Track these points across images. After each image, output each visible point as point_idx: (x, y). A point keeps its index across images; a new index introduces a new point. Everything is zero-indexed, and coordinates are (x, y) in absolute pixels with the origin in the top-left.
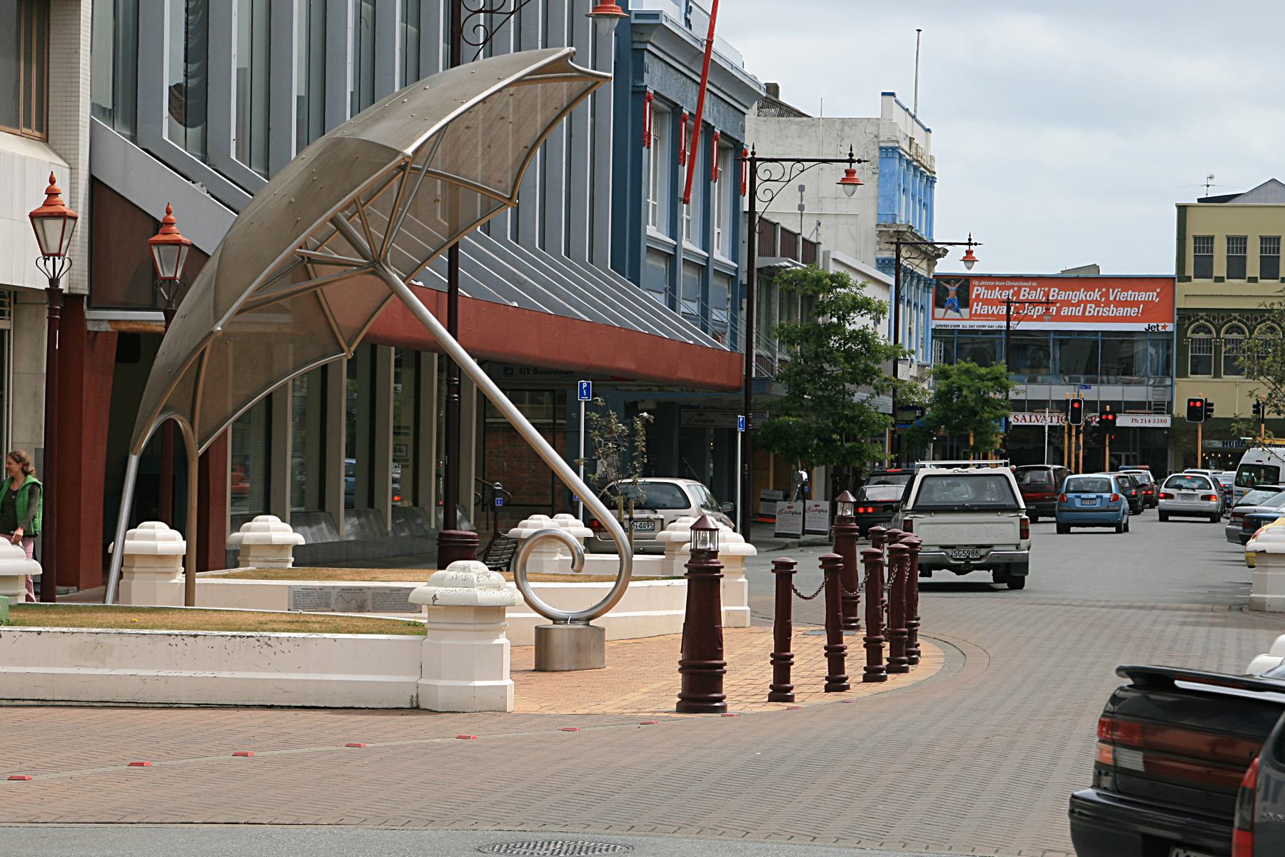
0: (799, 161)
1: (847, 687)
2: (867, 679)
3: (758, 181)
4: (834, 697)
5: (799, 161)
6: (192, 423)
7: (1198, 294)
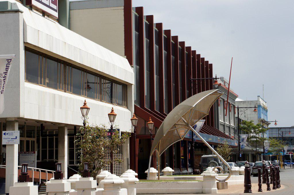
0: (246, 108)
1: (270, 190)
2: (273, 189)
3: (239, 111)
4: (268, 191)
5: (246, 108)
6: (158, 151)
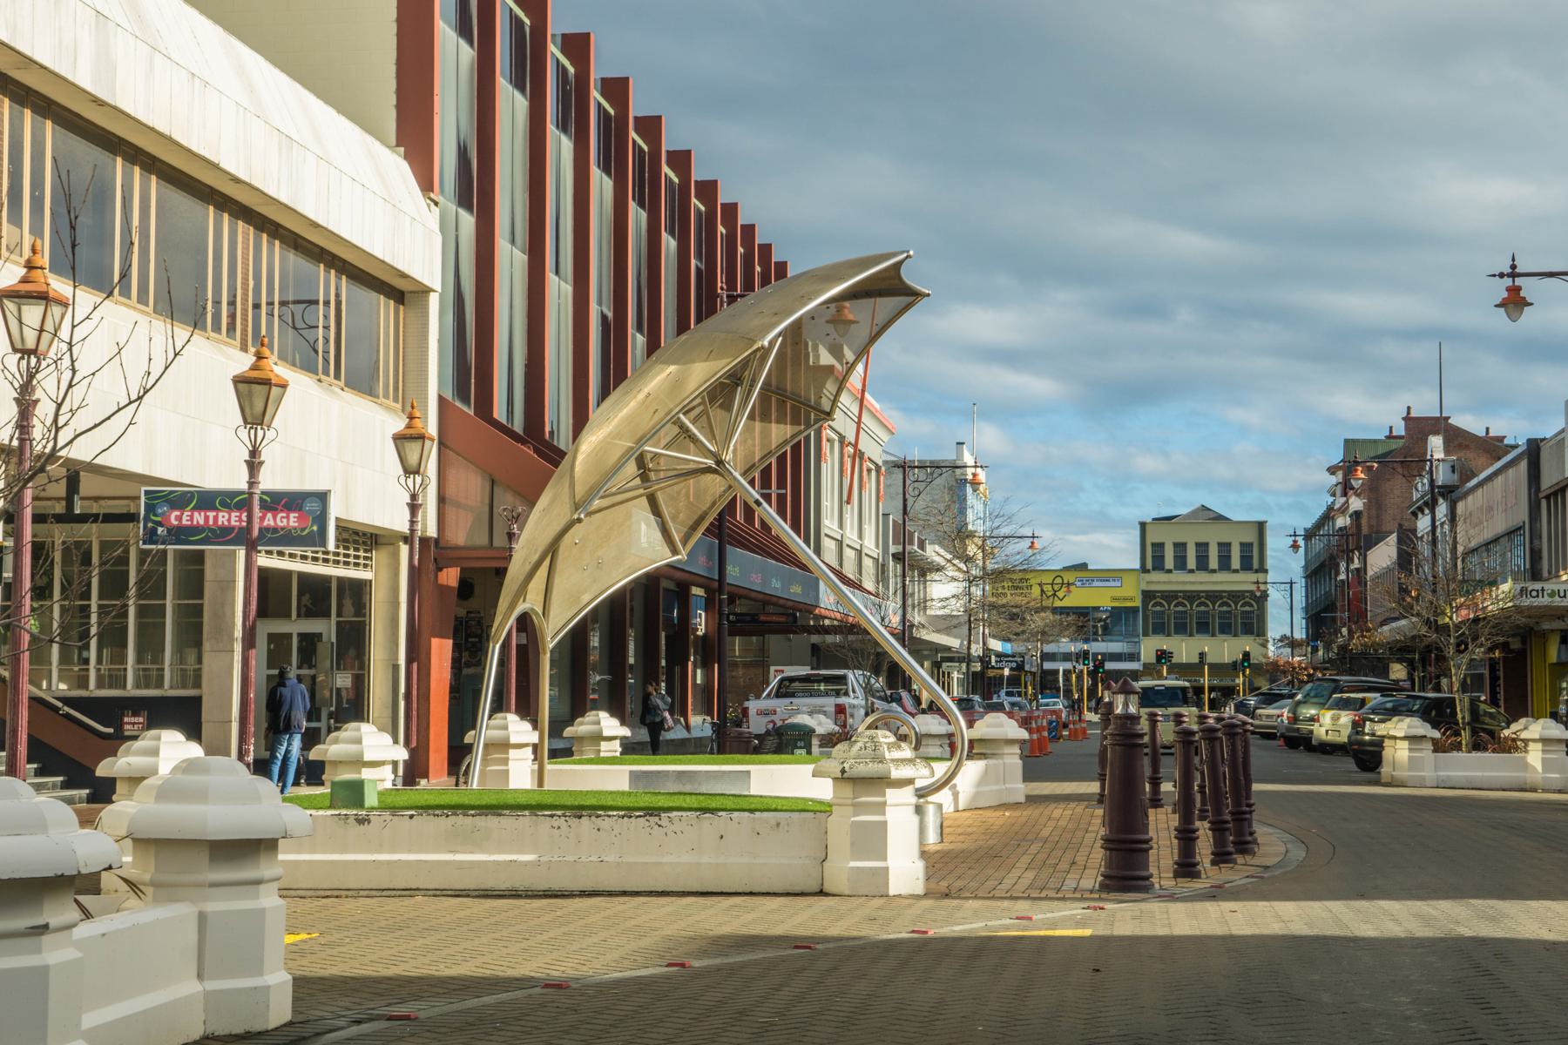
7: (1161, 581)
